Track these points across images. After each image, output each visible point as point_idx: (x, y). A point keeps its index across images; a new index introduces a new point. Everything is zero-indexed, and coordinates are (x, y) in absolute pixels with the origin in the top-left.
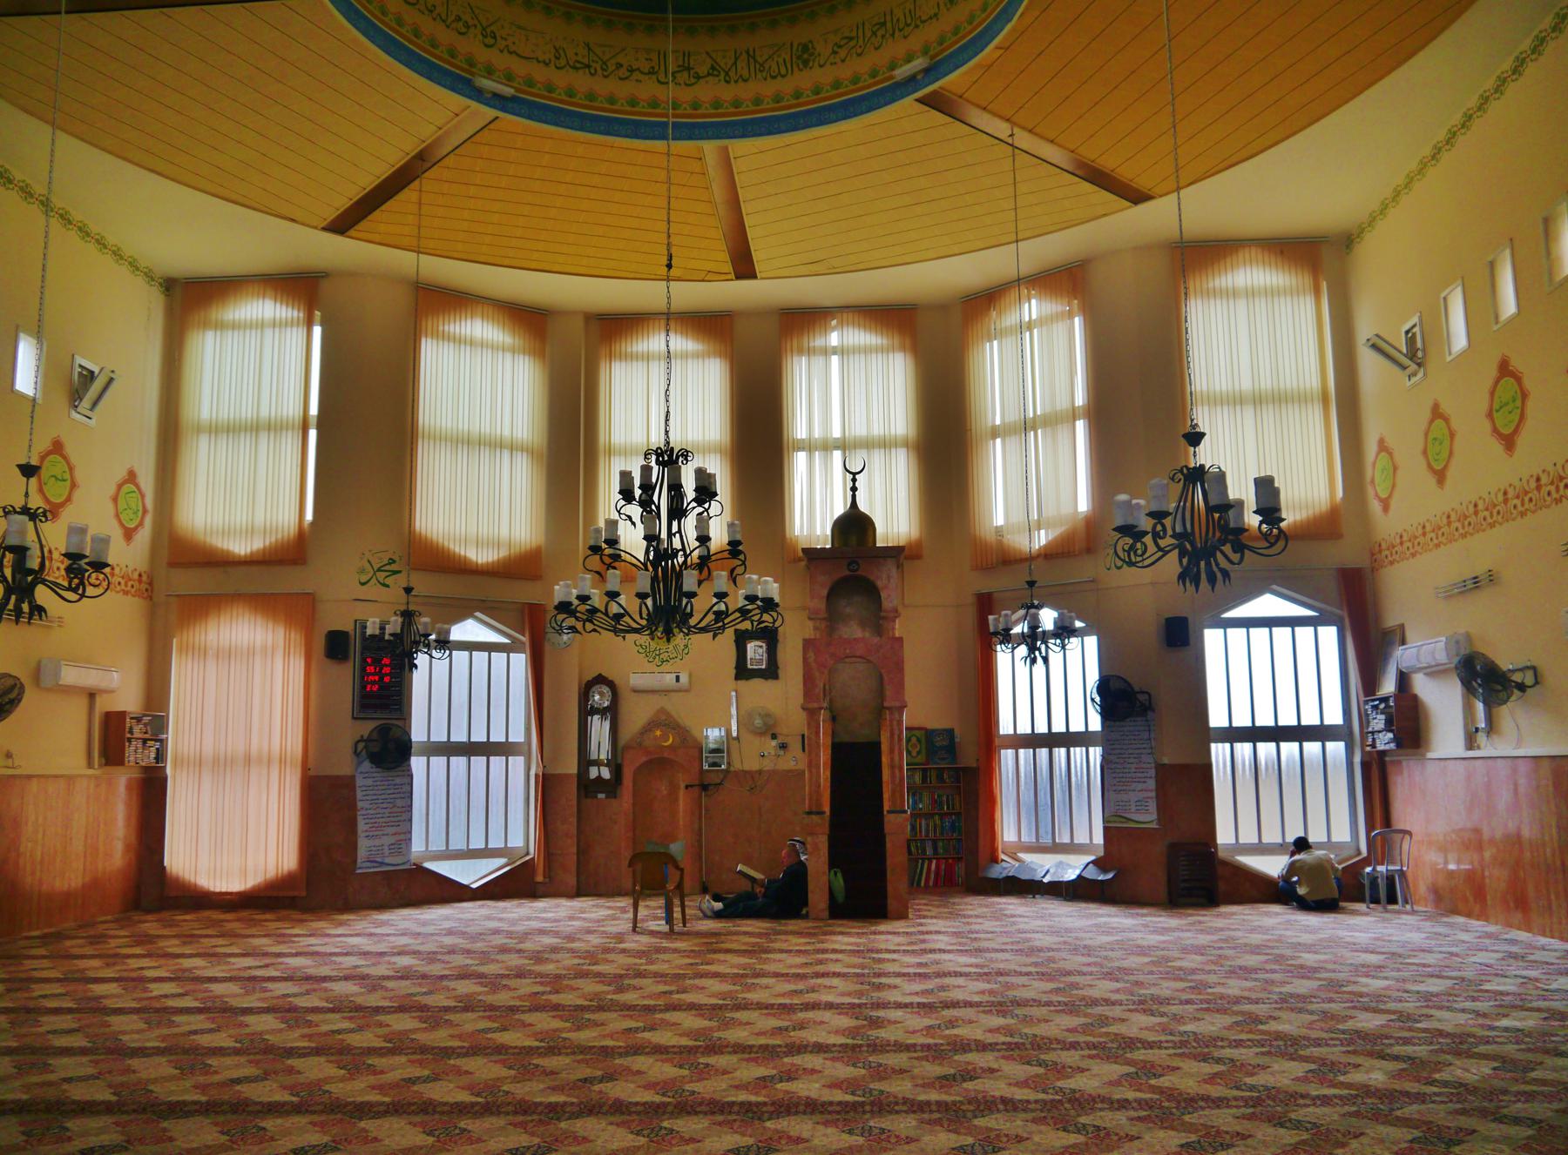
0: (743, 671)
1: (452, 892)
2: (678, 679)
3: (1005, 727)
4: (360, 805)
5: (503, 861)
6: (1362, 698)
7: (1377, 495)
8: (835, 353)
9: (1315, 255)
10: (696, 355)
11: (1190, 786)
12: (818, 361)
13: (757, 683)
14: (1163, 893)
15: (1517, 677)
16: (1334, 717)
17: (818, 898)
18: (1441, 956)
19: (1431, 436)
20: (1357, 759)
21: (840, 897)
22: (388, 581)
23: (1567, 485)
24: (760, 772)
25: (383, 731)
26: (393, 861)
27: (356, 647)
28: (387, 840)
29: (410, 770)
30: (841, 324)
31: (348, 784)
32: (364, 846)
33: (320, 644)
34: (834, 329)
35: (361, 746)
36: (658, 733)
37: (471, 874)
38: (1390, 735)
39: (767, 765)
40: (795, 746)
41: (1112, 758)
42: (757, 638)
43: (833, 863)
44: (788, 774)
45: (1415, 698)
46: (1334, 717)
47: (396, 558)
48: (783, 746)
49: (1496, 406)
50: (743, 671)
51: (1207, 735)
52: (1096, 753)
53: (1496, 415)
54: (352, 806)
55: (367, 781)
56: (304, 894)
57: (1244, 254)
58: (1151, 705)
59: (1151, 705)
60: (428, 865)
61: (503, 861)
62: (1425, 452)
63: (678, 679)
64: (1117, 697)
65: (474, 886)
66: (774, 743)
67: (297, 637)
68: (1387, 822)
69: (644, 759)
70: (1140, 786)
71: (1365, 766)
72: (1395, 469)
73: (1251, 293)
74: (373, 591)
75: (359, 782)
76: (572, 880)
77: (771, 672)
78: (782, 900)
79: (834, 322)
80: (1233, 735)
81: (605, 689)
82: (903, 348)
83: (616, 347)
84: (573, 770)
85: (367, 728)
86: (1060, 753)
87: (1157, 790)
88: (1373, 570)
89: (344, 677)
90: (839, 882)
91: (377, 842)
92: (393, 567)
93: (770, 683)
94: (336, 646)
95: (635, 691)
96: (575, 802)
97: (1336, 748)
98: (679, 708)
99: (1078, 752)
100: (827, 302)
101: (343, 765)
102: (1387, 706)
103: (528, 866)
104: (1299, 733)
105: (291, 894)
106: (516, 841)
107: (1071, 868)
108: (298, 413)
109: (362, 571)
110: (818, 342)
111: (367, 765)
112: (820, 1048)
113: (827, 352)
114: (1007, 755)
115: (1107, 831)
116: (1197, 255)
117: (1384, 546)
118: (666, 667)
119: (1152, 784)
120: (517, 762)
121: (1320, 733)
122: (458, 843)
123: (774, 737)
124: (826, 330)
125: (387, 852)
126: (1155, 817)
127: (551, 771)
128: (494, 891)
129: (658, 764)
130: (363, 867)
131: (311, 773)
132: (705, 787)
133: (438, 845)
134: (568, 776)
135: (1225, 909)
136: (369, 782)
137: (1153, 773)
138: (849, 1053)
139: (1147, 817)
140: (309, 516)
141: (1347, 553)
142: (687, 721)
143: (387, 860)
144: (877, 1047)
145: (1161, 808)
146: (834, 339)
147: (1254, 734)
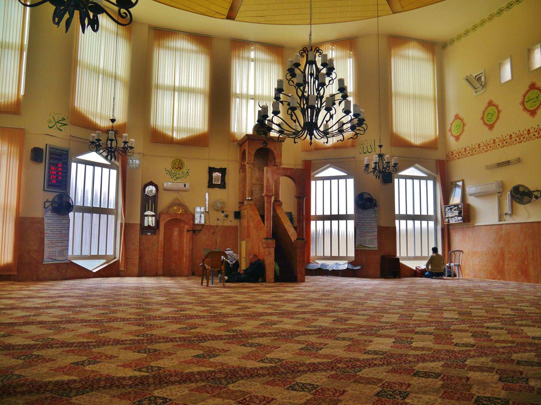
0: (211, 185)
1: (86, 274)
2: (185, 186)
3: (313, 213)
4: (46, 231)
5: (104, 261)
6: (443, 206)
7: (452, 135)
8: (252, 61)
9: (436, 48)
10: (197, 52)
11: (388, 234)
12: (245, 63)
13: (217, 190)
14: (378, 273)
15: (536, 193)
16: (431, 213)
17: (270, 273)
18: (352, 303)
19: (486, 113)
20: (439, 227)
21: (278, 274)
22: (61, 128)
23: (540, 133)
24: (217, 226)
25: (60, 197)
26: (60, 259)
27: (46, 156)
28: (58, 249)
29: (69, 217)
30: (255, 49)
31: (41, 221)
32: (47, 251)
33: (28, 154)
34: (252, 50)
35: (47, 204)
36: (175, 208)
37: (93, 266)
38: (461, 218)
39: (220, 223)
40: (232, 216)
41: (359, 224)
42: (218, 172)
43: (276, 260)
44: (228, 228)
45: (469, 205)
46: (431, 213)
47: (66, 118)
48: (227, 216)
49: (526, 100)
50: (211, 185)
51: (394, 217)
52: (351, 224)
53: (525, 103)
54: (43, 233)
55: (50, 221)
56: (16, 273)
57: (412, 44)
58: (373, 204)
59: (373, 204)
60: (73, 261)
61: (104, 261)
62: (483, 118)
63: (185, 186)
64: (364, 202)
65: (94, 271)
66: (223, 215)
67: (15, 150)
68: (449, 249)
69: (169, 219)
70: (371, 234)
71: (443, 230)
72: (464, 125)
73: (414, 58)
74: (54, 131)
75: (46, 220)
76: (136, 270)
77: (223, 186)
78: (255, 273)
79: (252, 48)
80: (407, 217)
81: (147, 189)
82: (278, 63)
83: (162, 42)
84: (138, 221)
85: (51, 196)
86: (335, 223)
87: (378, 236)
88: (447, 161)
89: (39, 172)
90: (278, 268)
91: (53, 250)
92: (64, 122)
93: (222, 190)
94: (37, 155)
95: (165, 190)
96: (138, 236)
97: (432, 224)
98: (185, 199)
99: (343, 223)
100: (252, 39)
101: (38, 212)
102: (458, 208)
103: (117, 263)
104: (421, 218)
105: (8, 273)
106: (110, 252)
107: (343, 265)
108: (18, 41)
109: (50, 122)
110: (246, 54)
111: (49, 214)
112: (117, 342)
113: (249, 59)
114: (313, 223)
115: (356, 251)
116: (397, 40)
117: (454, 152)
118: (178, 180)
119: (376, 234)
120: (112, 218)
121: (426, 218)
122: (86, 252)
123: (223, 212)
124: (249, 50)
125: (57, 254)
126: (377, 246)
127: (127, 222)
128: (103, 273)
129: (175, 221)
130: (46, 261)
131: (20, 216)
132: (194, 231)
133: (77, 253)
134: (135, 224)
135: (402, 279)
136: (50, 221)
137: (376, 230)
138: (135, 345)
139: (374, 245)
140: (22, 92)
141: (439, 155)
142: (187, 204)
143: (57, 259)
144: (152, 340)
145: (379, 243)
146: (252, 55)
147: (414, 218)
